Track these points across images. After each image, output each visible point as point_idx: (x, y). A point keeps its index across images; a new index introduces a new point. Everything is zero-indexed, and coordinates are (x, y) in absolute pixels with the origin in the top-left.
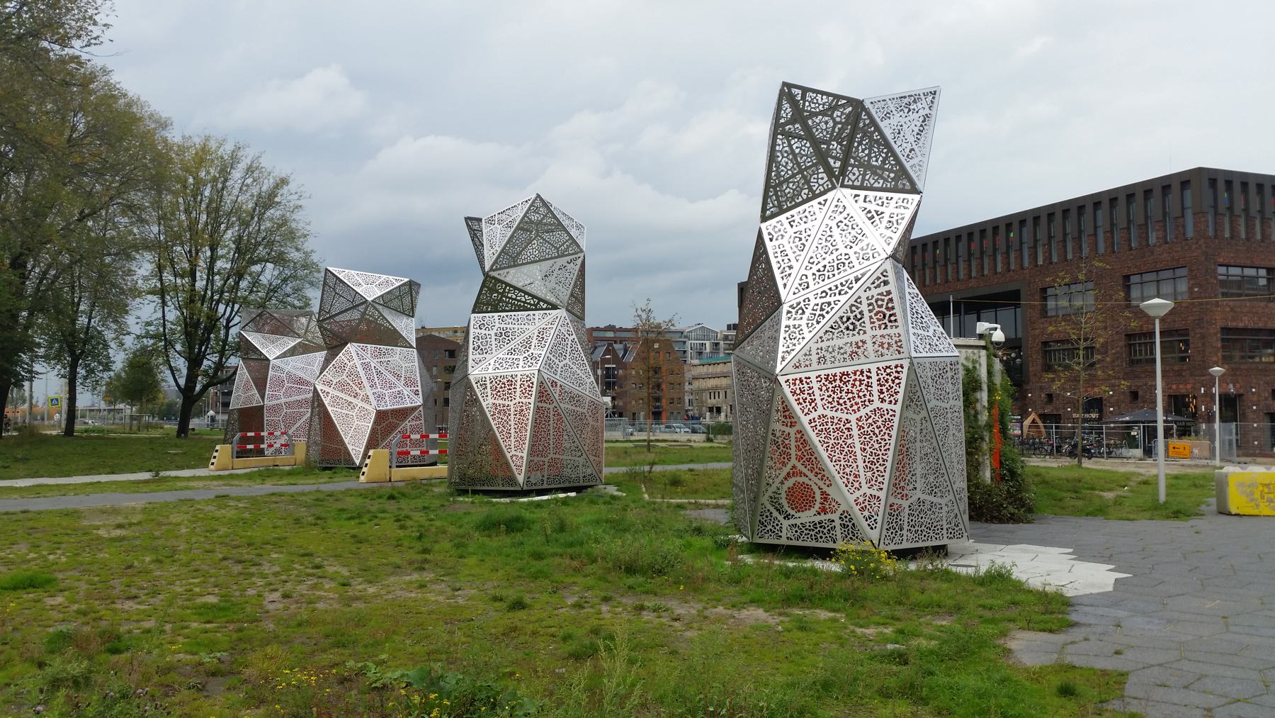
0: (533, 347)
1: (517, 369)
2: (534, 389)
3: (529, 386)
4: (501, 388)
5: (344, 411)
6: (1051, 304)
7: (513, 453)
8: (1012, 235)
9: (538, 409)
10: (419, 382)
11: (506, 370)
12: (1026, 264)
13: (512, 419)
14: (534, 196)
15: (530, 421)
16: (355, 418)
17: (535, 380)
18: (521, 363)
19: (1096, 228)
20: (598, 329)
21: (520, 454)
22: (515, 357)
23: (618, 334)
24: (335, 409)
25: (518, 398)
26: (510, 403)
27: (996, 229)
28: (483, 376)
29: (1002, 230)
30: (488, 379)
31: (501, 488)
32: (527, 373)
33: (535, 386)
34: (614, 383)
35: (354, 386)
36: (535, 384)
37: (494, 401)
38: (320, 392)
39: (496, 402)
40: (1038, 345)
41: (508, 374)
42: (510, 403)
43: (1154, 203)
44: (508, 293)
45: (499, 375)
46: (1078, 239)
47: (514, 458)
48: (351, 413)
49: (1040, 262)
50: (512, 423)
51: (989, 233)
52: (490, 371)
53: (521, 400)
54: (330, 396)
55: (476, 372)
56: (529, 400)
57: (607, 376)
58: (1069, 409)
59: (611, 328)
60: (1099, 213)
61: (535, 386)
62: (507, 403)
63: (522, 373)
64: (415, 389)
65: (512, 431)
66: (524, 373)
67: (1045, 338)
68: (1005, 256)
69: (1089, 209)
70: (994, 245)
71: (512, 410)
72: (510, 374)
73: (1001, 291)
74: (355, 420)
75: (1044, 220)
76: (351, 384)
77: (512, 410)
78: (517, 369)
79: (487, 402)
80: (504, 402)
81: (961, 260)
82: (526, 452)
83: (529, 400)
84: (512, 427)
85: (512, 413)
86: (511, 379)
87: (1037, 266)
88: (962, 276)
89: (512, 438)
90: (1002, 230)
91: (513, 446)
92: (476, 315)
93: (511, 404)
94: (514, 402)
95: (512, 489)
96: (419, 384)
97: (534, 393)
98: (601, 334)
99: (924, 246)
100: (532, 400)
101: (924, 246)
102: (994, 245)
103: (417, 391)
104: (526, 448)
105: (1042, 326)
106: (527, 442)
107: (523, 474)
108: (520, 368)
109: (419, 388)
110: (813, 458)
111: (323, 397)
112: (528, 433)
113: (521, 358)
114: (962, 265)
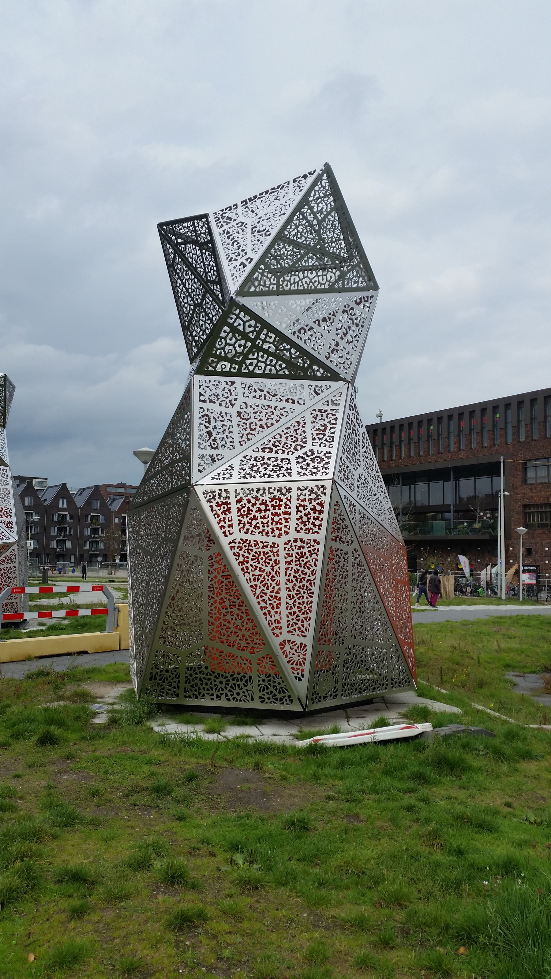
0: (309, 440)
1: (288, 478)
2: (325, 516)
3: (314, 510)
4: (260, 511)
6: (531, 474)
7: (286, 636)
8: (432, 428)
9: (330, 553)
10: (13, 511)
11: (266, 479)
12: (510, 440)
13: (282, 571)
14: (320, 168)
15: (318, 576)
17: (326, 499)
18: (295, 468)
20: (111, 486)
21: (299, 640)
22: (280, 456)
23: (129, 491)
25: (292, 531)
26: (276, 540)
27: (420, 423)
28: (223, 487)
29: (489, 411)
30: (232, 495)
31: (256, 705)
32: (311, 485)
33: (326, 510)
36: (326, 505)
37: (245, 537)
39: (249, 537)
40: (519, 507)
41: (272, 485)
42: (276, 540)
44: (264, 341)
45: (255, 486)
46: (517, 429)
47: (287, 648)
49: (523, 439)
50: (282, 578)
51: (406, 427)
52: (235, 478)
53: (299, 536)
55: (208, 480)
56: (315, 537)
58: (547, 562)
59: (122, 485)
60: (452, 423)
61: (326, 510)
62: (270, 540)
63: (300, 484)
64: (7, 520)
65: (283, 594)
66: (305, 484)
67: (526, 501)
68: (426, 443)
70: (409, 436)
71: (282, 553)
72: (277, 485)
73: (420, 469)
75: (415, 425)
77: (282, 553)
78: (288, 478)
79: (230, 538)
80: (264, 539)
81: (452, 435)
82: (310, 635)
83: (315, 537)
84: (283, 586)
85: (282, 559)
86: (277, 494)
87: (519, 442)
88: (452, 449)
89: (283, 608)
90: (489, 411)
91: (284, 624)
92: (203, 378)
93: (280, 542)
94: (285, 538)
95: (282, 707)
96: (13, 514)
97: (324, 523)
98: (114, 490)
99: (392, 428)
100: (321, 536)
101: (392, 428)
102: (409, 436)
103: (10, 522)
104: (312, 628)
105: (523, 491)
106: (313, 615)
107: (305, 680)
108: (295, 477)
109: (14, 520)
112: (315, 599)
113: (293, 458)
114: (452, 440)
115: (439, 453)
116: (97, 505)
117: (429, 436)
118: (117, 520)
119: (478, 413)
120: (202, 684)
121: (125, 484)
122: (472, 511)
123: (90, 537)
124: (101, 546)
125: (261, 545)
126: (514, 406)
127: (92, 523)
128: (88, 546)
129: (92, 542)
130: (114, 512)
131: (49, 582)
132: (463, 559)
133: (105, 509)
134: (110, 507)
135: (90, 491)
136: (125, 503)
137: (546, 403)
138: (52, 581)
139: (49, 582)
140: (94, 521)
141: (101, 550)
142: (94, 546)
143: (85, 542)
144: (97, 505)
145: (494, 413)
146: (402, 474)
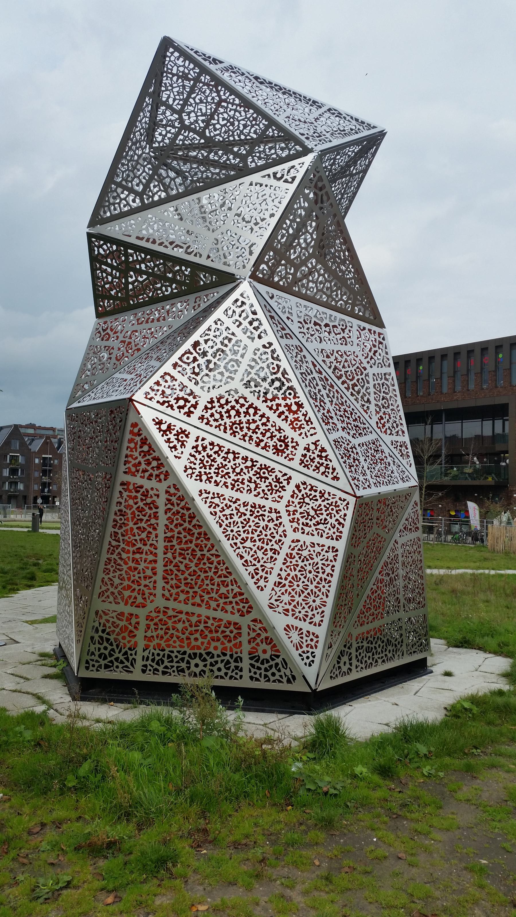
5: (244, 497)
16: (285, 519)
19: (442, 373)
23: (38, 432)
24: (211, 487)
29: (413, 363)
34: (50, 471)
35: (273, 417)
38: (153, 429)
43: (489, 358)
48: (268, 504)
54: (191, 442)
57: (44, 464)
69: (438, 359)
74: (288, 526)
76: (263, 408)
110: (154, 533)
111: (164, 447)
115: (429, 395)
116: (16, 445)
117: (418, 377)
118: (37, 461)
119: (478, 352)
120: (178, 652)
121: (34, 425)
122: (464, 455)
123: (9, 477)
124: (21, 487)
125: (309, 487)
126: (451, 357)
127: (11, 463)
128: (7, 487)
129: (11, 483)
130: (34, 452)
131: (40, 531)
132: (472, 506)
133: (24, 449)
134: (30, 447)
135: (9, 430)
136: (45, 443)
137: (511, 349)
138: (43, 528)
139: (40, 531)
140: (13, 461)
141: (20, 491)
142: (13, 487)
143: (4, 483)
144: (16, 445)
145: (418, 365)
146: (444, 410)
